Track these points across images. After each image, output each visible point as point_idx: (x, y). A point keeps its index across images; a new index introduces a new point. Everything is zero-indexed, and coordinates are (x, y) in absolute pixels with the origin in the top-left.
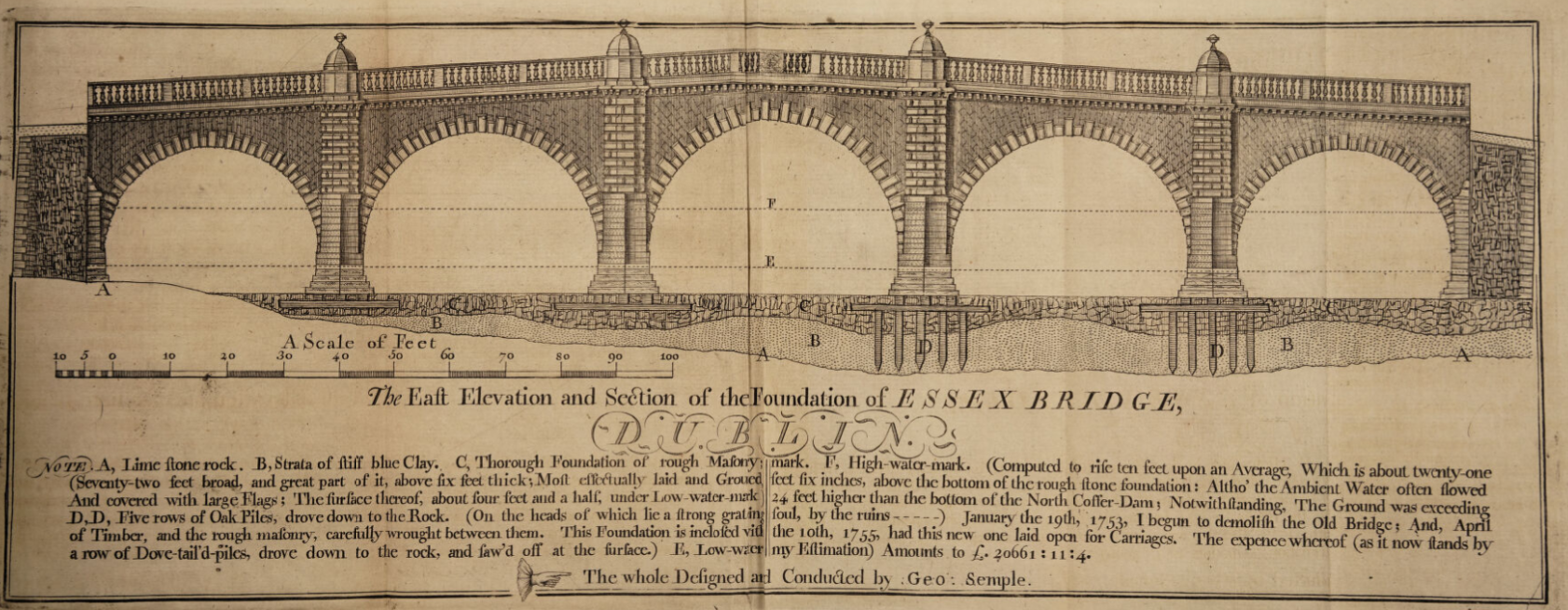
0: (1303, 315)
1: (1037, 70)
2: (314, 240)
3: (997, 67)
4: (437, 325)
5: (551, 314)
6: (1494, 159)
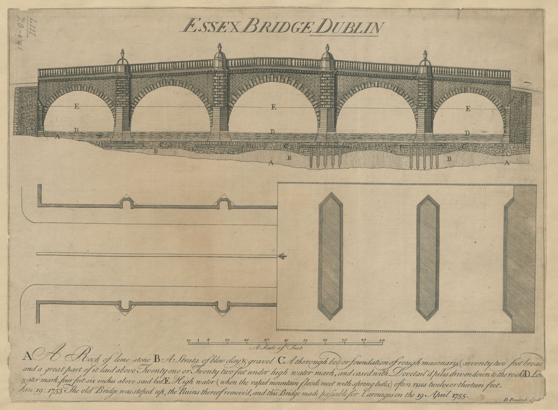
0: (455, 149)
1: (365, 65)
2: (114, 123)
3: (351, 64)
4: (156, 152)
5: (195, 148)
6: (518, 96)
